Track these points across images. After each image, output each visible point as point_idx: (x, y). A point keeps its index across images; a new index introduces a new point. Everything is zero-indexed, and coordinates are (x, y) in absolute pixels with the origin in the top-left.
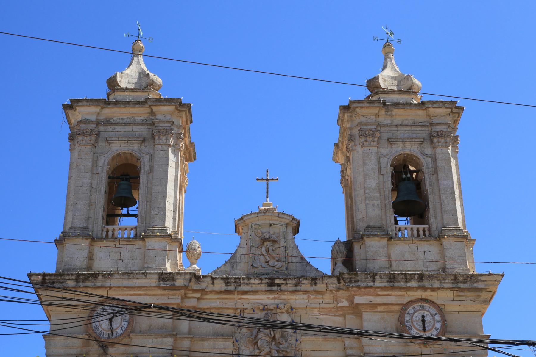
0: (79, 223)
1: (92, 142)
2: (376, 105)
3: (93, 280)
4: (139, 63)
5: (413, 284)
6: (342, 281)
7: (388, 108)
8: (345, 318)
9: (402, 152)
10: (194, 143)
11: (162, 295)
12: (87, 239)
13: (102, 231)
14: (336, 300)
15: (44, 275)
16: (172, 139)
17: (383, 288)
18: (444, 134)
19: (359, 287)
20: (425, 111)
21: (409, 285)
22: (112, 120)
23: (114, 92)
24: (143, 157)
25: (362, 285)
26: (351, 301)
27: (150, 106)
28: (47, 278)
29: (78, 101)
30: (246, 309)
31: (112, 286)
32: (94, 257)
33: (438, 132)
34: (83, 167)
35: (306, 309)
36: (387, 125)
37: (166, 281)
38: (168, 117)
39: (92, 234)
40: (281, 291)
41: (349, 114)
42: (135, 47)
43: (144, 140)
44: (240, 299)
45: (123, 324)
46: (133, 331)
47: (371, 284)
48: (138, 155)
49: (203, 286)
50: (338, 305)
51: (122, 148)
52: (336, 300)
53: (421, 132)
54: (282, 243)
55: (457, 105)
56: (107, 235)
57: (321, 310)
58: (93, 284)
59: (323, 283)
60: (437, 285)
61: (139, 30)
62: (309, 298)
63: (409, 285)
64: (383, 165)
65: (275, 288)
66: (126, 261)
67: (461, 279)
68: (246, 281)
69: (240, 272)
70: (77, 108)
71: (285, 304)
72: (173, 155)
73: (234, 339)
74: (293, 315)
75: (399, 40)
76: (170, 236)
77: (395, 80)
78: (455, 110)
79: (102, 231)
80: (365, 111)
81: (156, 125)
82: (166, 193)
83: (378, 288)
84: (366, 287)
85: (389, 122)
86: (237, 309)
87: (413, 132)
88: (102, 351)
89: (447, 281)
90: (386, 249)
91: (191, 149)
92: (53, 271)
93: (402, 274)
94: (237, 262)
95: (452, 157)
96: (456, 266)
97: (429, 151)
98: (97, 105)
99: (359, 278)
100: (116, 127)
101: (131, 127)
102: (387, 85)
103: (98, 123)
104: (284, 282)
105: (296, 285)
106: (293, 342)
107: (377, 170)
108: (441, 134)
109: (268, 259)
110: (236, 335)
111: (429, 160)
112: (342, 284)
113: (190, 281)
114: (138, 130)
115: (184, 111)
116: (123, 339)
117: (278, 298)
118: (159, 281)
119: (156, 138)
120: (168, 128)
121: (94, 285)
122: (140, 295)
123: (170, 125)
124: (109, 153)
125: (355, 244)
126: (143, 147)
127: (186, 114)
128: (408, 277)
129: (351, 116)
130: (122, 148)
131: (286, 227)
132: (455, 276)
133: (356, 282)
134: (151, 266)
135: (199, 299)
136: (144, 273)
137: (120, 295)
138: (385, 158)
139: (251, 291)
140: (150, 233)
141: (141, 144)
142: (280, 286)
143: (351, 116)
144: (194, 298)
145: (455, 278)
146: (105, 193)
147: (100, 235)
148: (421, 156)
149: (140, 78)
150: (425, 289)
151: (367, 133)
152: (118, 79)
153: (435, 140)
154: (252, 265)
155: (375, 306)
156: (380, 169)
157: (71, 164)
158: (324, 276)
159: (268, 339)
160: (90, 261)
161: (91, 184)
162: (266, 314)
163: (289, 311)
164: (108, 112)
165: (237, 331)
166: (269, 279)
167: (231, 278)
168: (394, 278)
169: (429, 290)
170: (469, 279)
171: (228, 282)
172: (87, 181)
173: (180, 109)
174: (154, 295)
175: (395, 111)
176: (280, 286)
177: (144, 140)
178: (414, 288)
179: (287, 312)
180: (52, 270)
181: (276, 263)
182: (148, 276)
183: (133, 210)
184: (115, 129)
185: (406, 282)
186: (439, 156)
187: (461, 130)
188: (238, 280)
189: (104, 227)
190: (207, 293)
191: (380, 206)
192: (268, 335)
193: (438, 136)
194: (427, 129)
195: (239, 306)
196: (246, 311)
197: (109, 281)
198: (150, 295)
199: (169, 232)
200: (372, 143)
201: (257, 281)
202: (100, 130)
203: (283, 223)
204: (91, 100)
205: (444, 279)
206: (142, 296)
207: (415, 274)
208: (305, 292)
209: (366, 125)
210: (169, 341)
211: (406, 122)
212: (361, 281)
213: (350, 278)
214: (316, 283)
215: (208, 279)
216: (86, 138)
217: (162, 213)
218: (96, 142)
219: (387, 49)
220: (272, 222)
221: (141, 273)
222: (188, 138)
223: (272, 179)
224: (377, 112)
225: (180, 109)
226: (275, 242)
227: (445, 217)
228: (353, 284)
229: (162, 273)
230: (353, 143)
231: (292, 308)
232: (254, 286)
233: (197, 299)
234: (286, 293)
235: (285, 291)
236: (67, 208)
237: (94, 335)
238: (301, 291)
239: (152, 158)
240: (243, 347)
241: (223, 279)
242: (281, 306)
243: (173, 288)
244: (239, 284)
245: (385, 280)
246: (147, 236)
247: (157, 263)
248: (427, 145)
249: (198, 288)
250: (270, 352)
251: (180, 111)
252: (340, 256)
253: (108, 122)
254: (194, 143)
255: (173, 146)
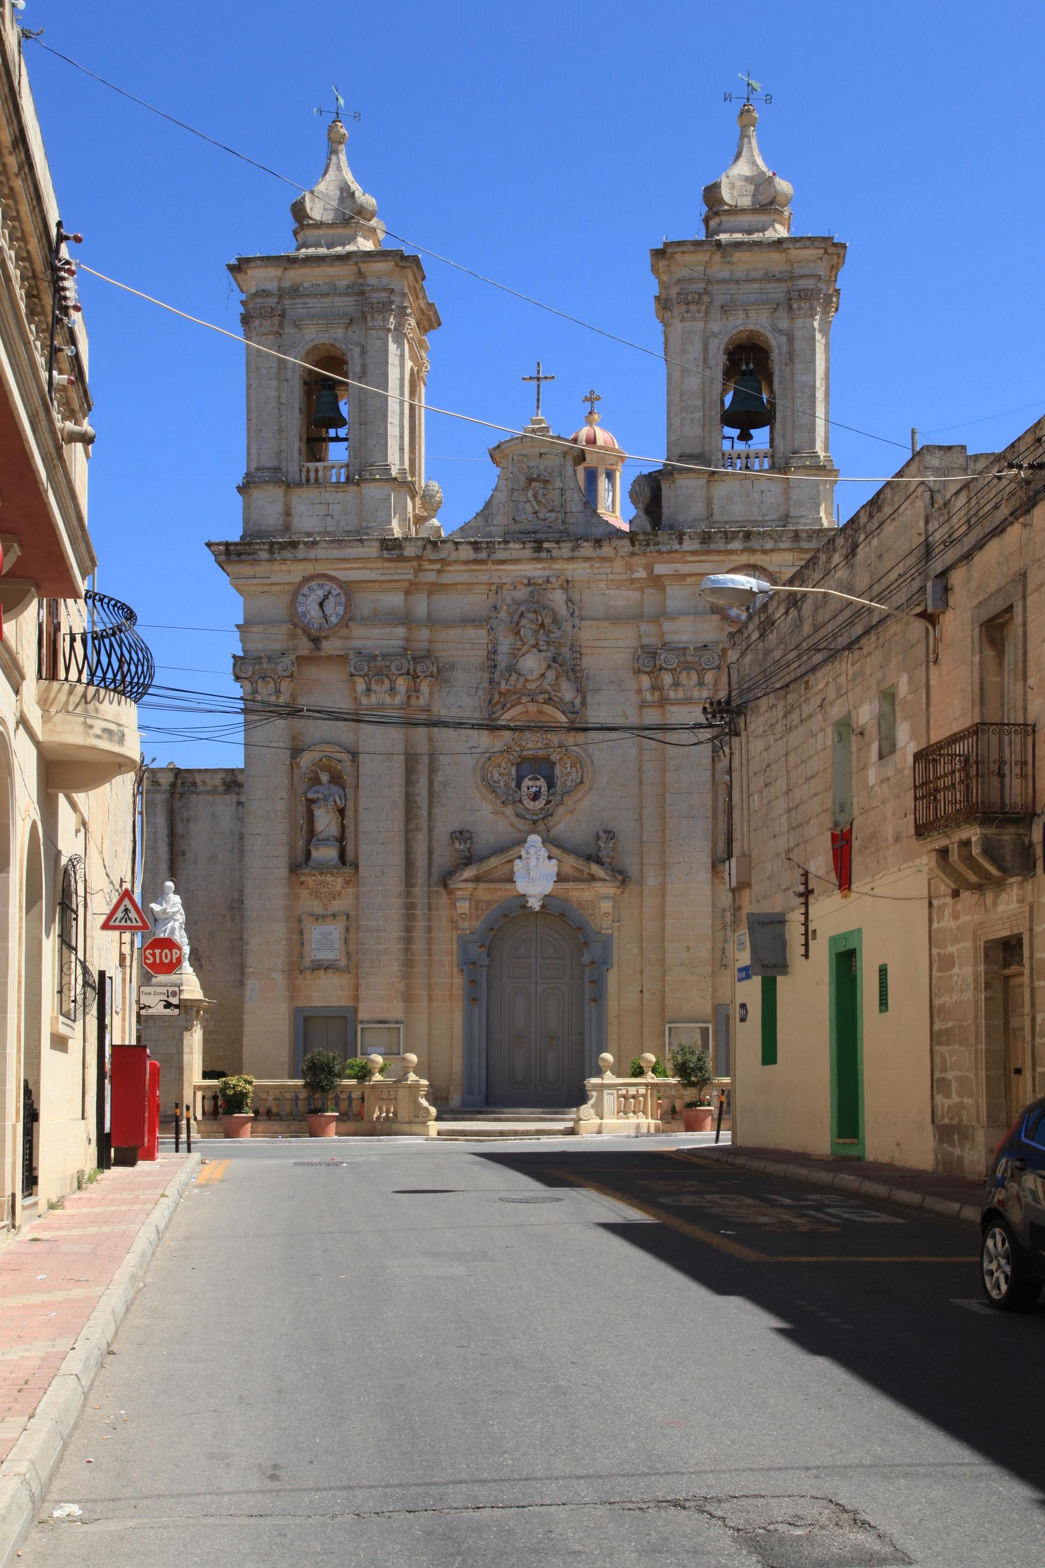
0: (268, 462)
1: (275, 329)
2: (706, 248)
3: (292, 551)
4: (339, 169)
5: (737, 545)
6: (637, 543)
7: (725, 250)
8: (643, 592)
9: (742, 328)
10: (433, 304)
11: (388, 568)
12: (280, 486)
13: (301, 471)
14: (630, 568)
15: (227, 544)
16: (392, 319)
17: (693, 553)
18: (809, 294)
19: (659, 552)
20: (784, 254)
21: (730, 547)
22: (301, 288)
23: (303, 229)
24: (350, 350)
25: (664, 549)
26: (650, 569)
27: (356, 263)
28: (232, 548)
29: (248, 260)
30: (504, 584)
31: (318, 557)
32: (293, 512)
33: (800, 291)
34: (265, 371)
35: (588, 581)
36: (722, 281)
37: (392, 550)
38: (385, 280)
39: (287, 479)
40: (552, 558)
41: (665, 263)
42: (333, 136)
43: (351, 321)
44: (496, 570)
45: (337, 610)
46: (351, 619)
47: (677, 547)
48: (344, 347)
49: (443, 554)
50: (633, 576)
51: (320, 336)
52: (630, 568)
53: (776, 290)
54: (558, 483)
55: (835, 241)
56: (308, 481)
57: (609, 583)
58: (293, 555)
59: (611, 546)
60: (769, 545)
61: (337, 99)
62: (592, 567)
63: (730, 547)
64: (712, 352)
65: (543, 555)
66: (336, 517)
67: (804, 535)
68: (502, 546)
69: (497, 528)
70: (248, 270)
71: (558, 577)
72: (395, 346)
73: (489, 627)
74: (570, 591)
75: (769, 97)
76: (395, 479)
77: (751, 183)
78: (831, 250)
79: (301, 471)
80: (689, 258)
81: (367, 295)
82: (387, 409)
83: (687, 552)
84: (670, 552)
85: (726, 274)
86: (493, 584)
87: (763, 291)
88: (313, 646)
89: (784, 539)
90: (704, 490)
91: (431, 313)
92: (237, 539)
93: (721, 532)
94: (492, 514)
95: (820, 331)
96: (804, 513)
97: (784, 324)
98: (277, 266)
99: (660, 539)
100: (308, 300)
101: (329, 300)
102: (736, 194)
103: (282, 293)
104: (555, 546)
105: (573, 550)
106: (569, 629)
107: (702, 360)
108: (806, 295)
109: (537, 508)
110: (492, 621)
111: (784, 339)
112: (637, 548)
113: (424, 549)
114: (342, 304)
115: (409, 267)
116: (339, 630)
117: (549, 569)
118: (382, 550)
119: (369, 318)
120: (385, 300)
121: (295, 557)
122: (358, 569)
123: (387, 295)
124: (301, 346)
125: (662, 482)
126: (350, 333)
127: (413, 271)
128: (729, 536)
129: (668, 266)
130: (320, 336)
131: (564, 457)
132: (796, 532)
133: (655, 544)
134: (371, 525)
135: (439, 571)
136: (359, 540)
137: (331, 569)
138: (716, 339)
139: (511, 560)
140: (368, 476)
141: (347, 328)
142: (550, 551)
143: (668, 266)
144: (432, 570)
145: (796, 536)
146: (301, 412)
147: (297, 478)
148: (772, 333)
149: (341, 199)
150: (752, 551)
151: (690, 297)
152: (308, 205)
153: (795, 306)
154: (513, 519)
155: (683, 577)
156: (705, 359)
157: (248, 363)
158: (618, 533)
159: (534, 627)
160: (287, 518)
161: (279, 397)
162: (532, 592)
163: (565, 585)
164: (294, 275)
165: (492, 615)
166: (535, 542)
167: (481, 542)
168: (710, 537)
169: (759, 553)
170: (815, 535)
171: (478, 548)
172: (273, 393)
173: (402, 264)
174: (377, 569)
175: (738, 256)
176: (550, 551)
177: (351, 321)
178: (737, 550)
179: (561, 587)
180: (235, 537)
181: (548, 515)
182: (366, 544)
183: (342, 432)
184: (306, 304)
185: (727, 543)
186: (798, 333)
187: (844, 279)
188: (491, 545)
189: (303, 466)
190: (449, 563)
191: (702, 421)
192: (533, 622)
193: (800, 298)
194: (784, 285)
195: (496, 580)
196: (505, 587)
197: (314, 551)
198: (371, 569)
199: (394, 472)
200: (697, 315)
201: (518, 546)
202: (286, 307)
203: (559, 452)
204: (268, 258)
205: (780, 537)
206: (361, 571)
207: (739, 532)
208: (587, 559)
209: (690, 284)
210: (401, 631)
211: (754, 274)
212: (663, 543)
213: (648, 540)
214: (600, 547)
215: (450, 545)
216: (265, 322)
217: (383, 442)
218: (281, 326)
219: (745, 119)
220: (543, 451)
221: (356, 540)
222: (423, 298)
223: (546, 378)
224: (707, 259)
225: (402, 264)
226: (546, 482)
227: (796, 435)
228: (651, 548)
229: (385, 539)
230: (669, 313)
231: (568, 582)
232: (514, 552)
233: (435, 573)
234: (560, 561)
235: (558, 559)
236: (249, 436)
237: (301, 625)
238: (580, 558)
239: (364, 352)
240: (501, 638)
241: (470, 543)
242: (553, 580)
243: (401, 558)
244: (493, 551)
245: (697, 541)
246: (362, 480)
247: (379, 520)
248: (782, 313)
249: (436, 558)
250: (537, 644)
251: (403, 267)
252: (641, 500)
253: (295, 291)
254: (433, 304)
255: (396, 329)
